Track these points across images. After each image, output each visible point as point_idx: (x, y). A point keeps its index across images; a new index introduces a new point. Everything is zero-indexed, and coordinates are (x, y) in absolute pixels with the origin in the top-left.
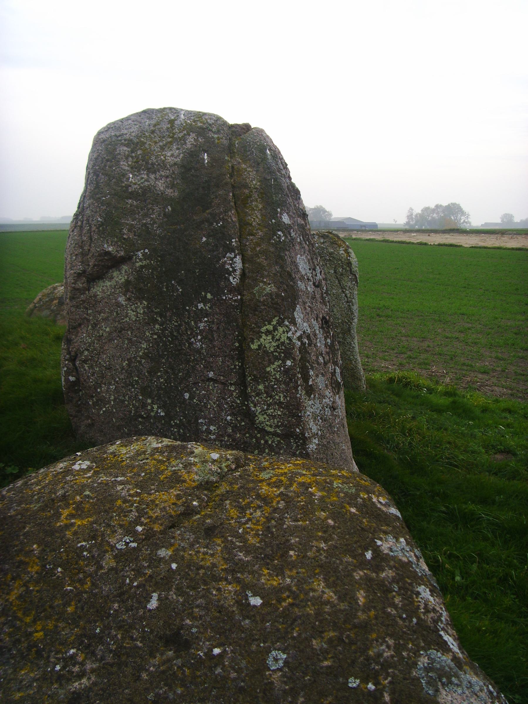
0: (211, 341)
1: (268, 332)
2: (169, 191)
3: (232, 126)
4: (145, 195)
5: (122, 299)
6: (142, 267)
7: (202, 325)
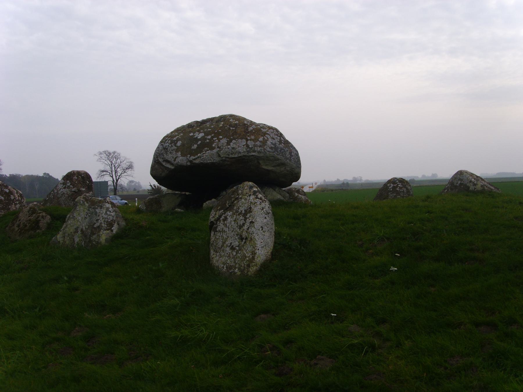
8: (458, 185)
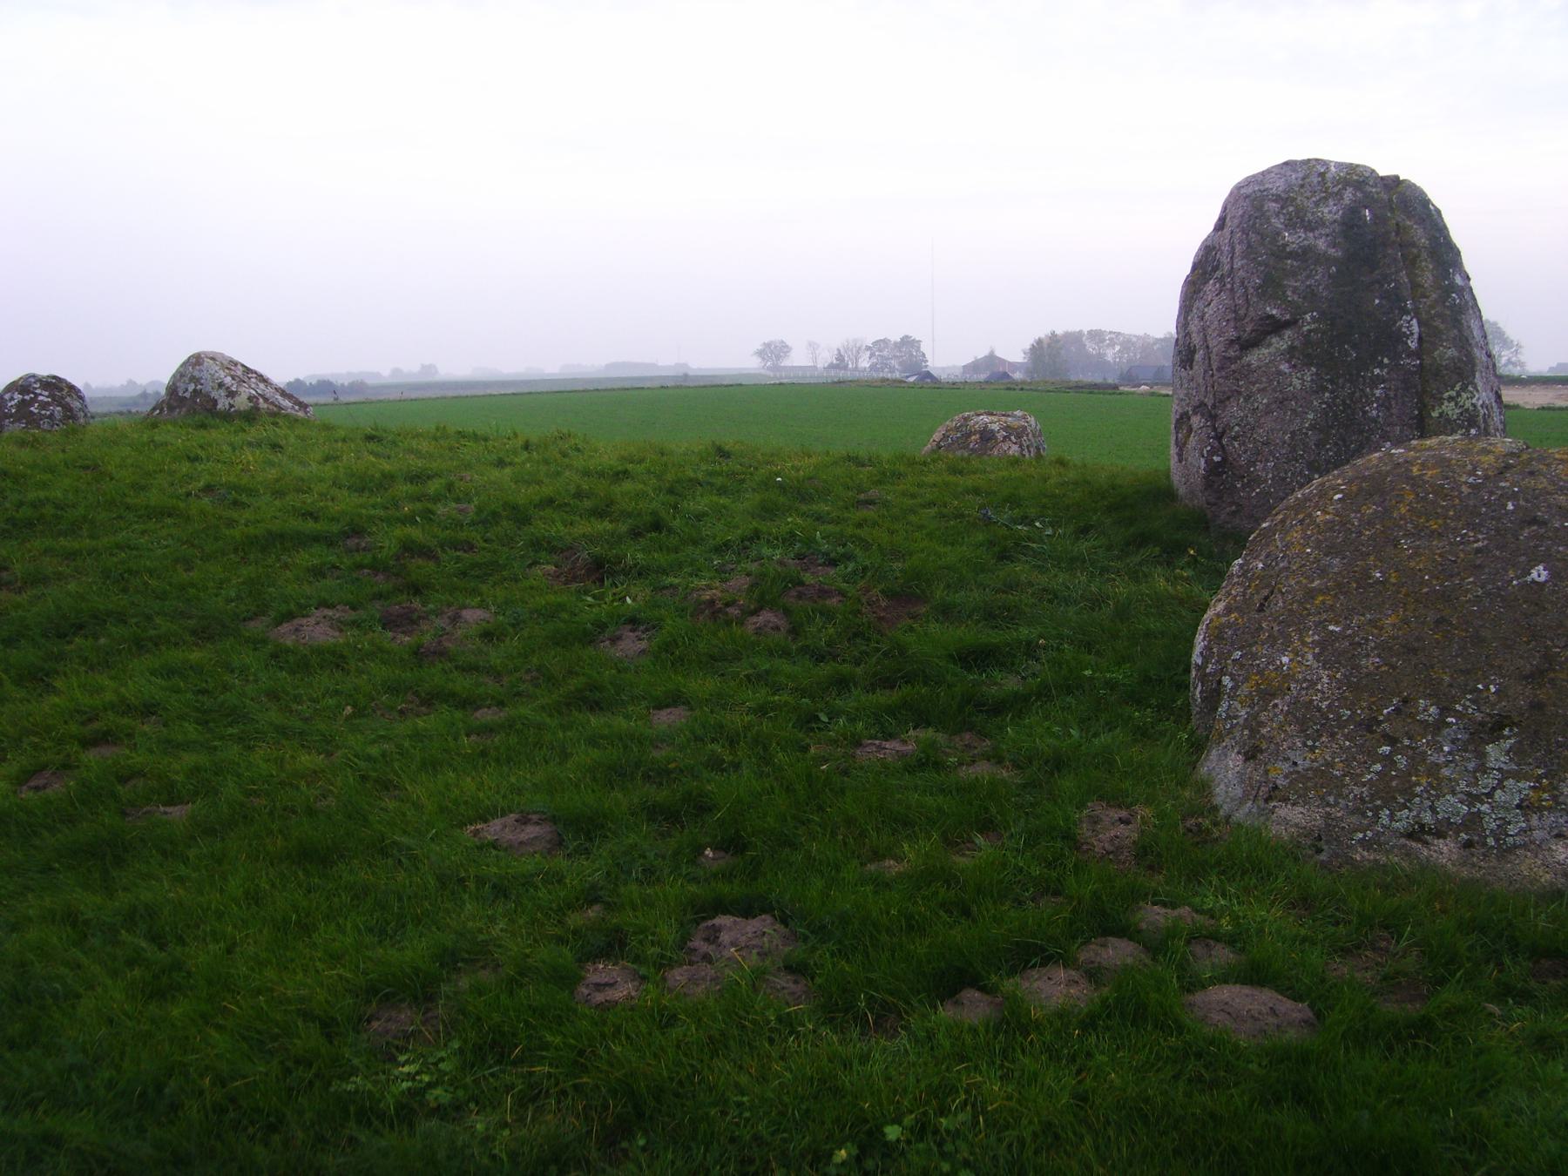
0: (1388, 409)
1: (1451, 399)
2: (1331, 251)
3: (1382, 178)
4: (1305, 255)
5: (1284, 367)
6: (1310, 331)
7: (1378, 392)
8: (187, 395)
